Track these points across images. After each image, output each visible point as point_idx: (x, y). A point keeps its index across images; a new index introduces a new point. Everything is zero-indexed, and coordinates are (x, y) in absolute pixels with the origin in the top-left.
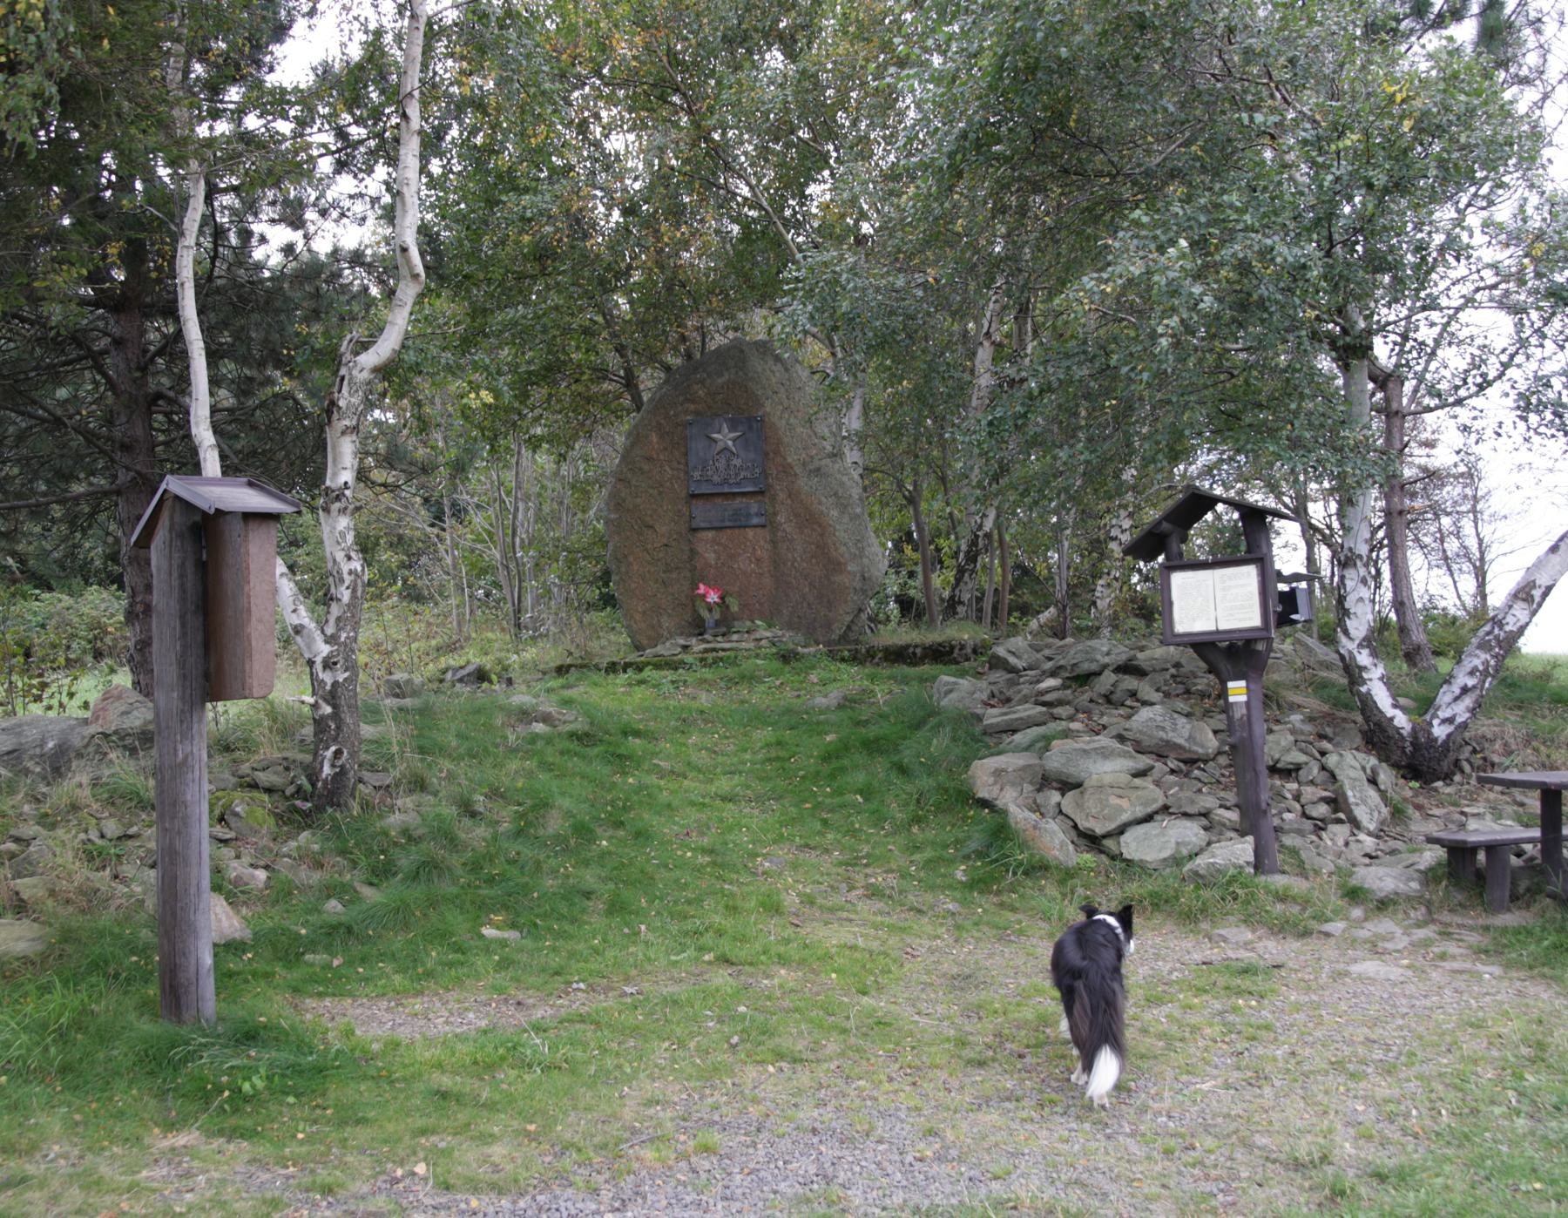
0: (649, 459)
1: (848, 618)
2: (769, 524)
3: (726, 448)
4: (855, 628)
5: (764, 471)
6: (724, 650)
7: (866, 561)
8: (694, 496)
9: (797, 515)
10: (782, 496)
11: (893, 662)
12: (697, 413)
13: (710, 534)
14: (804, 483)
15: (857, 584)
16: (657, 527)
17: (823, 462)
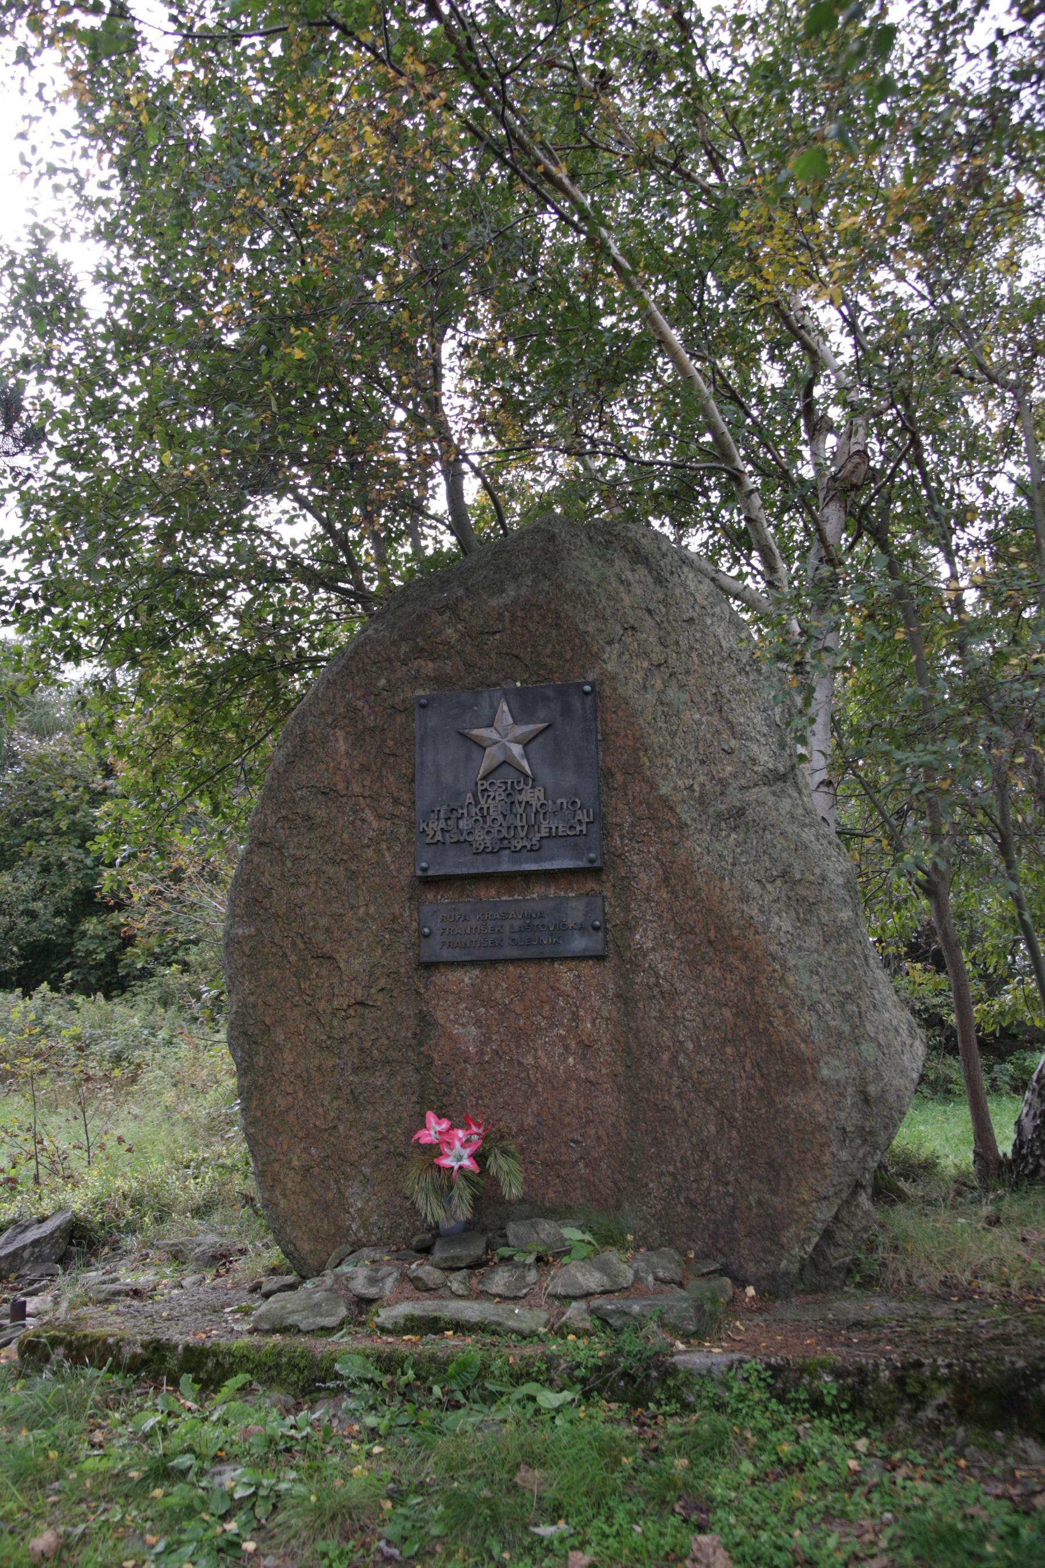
0: (327, 793)
1: (825, 1213)
2: (610, 950)
3: (507, 763)
4: (844, 1236)
5: (600, 818)
6: (460, 1327)
7: (868, 1050)
8: (429, 882)
9: (683, 931)
10: (645, 879)
11: (988, 1424)
12: (440, 681)
13: (467, 977)
14: (704, 848)
15: (848, 1116)
16: (341, 957)
17: (753, 794)
